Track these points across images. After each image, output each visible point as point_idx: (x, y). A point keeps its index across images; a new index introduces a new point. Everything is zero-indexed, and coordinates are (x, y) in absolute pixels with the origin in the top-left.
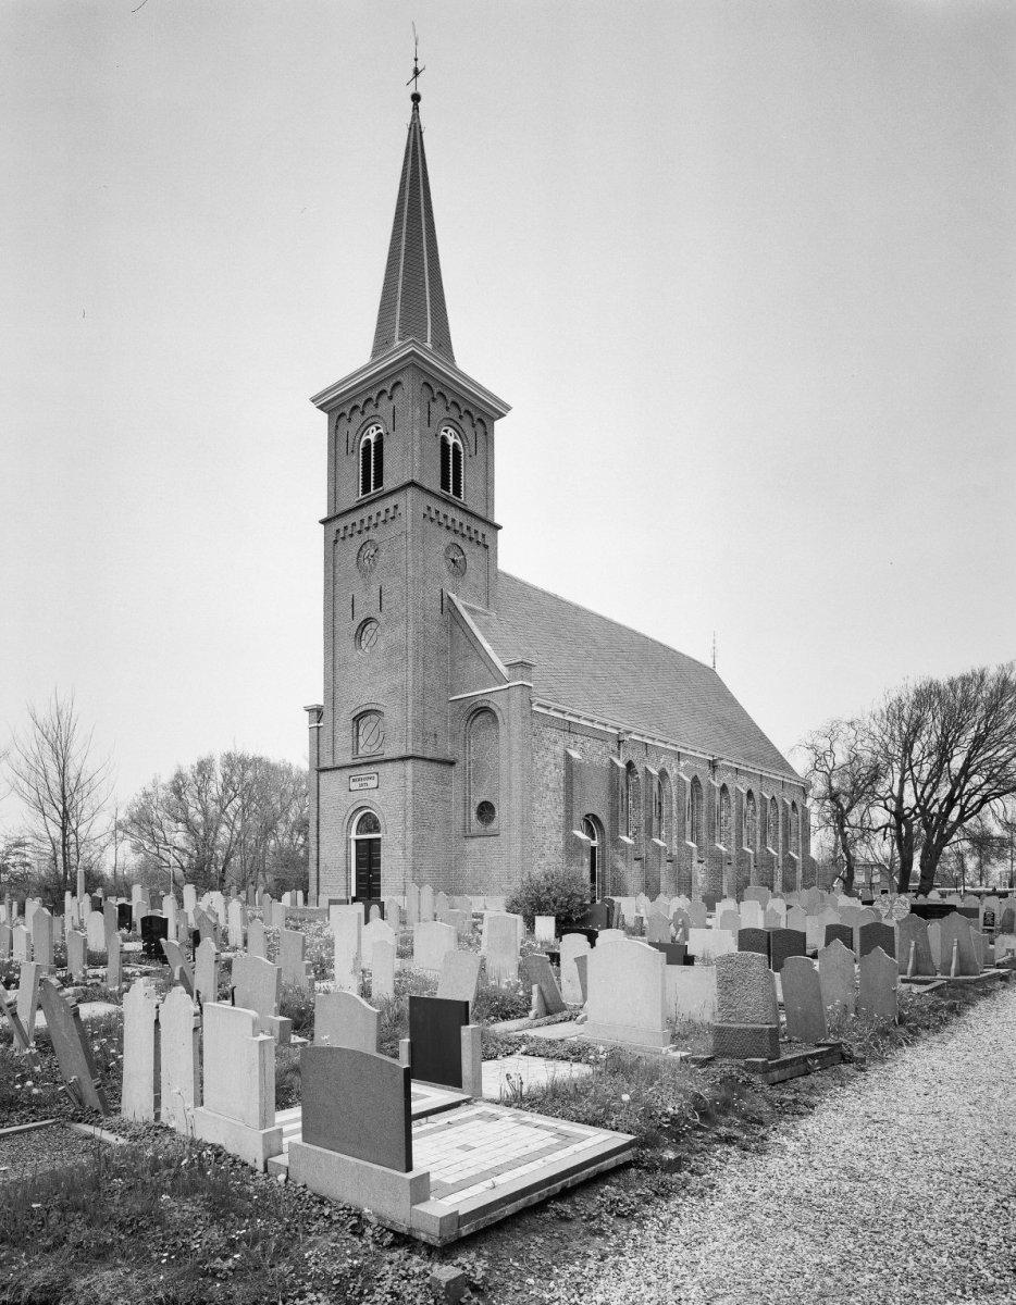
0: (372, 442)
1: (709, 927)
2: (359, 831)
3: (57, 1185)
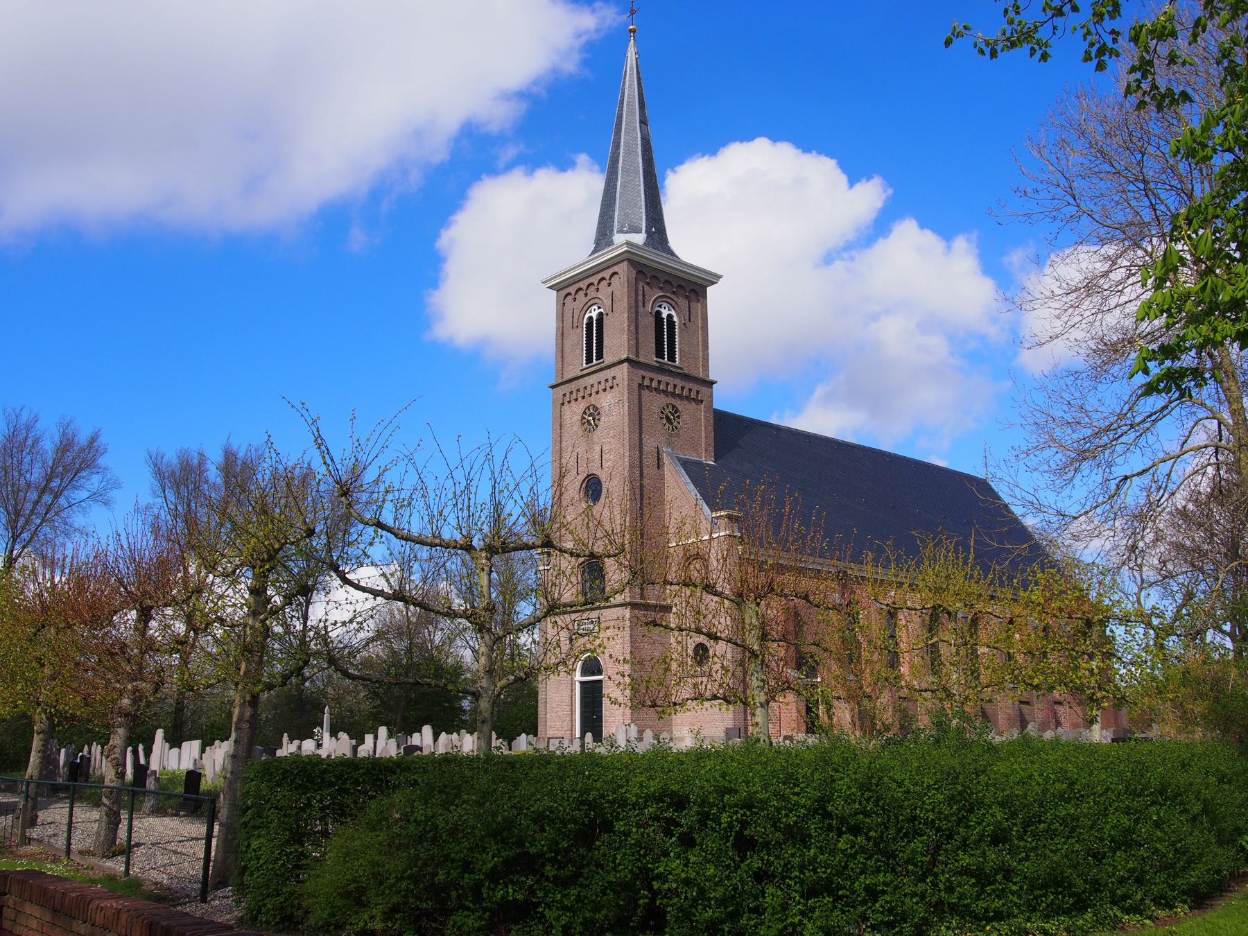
2: (584, 673)
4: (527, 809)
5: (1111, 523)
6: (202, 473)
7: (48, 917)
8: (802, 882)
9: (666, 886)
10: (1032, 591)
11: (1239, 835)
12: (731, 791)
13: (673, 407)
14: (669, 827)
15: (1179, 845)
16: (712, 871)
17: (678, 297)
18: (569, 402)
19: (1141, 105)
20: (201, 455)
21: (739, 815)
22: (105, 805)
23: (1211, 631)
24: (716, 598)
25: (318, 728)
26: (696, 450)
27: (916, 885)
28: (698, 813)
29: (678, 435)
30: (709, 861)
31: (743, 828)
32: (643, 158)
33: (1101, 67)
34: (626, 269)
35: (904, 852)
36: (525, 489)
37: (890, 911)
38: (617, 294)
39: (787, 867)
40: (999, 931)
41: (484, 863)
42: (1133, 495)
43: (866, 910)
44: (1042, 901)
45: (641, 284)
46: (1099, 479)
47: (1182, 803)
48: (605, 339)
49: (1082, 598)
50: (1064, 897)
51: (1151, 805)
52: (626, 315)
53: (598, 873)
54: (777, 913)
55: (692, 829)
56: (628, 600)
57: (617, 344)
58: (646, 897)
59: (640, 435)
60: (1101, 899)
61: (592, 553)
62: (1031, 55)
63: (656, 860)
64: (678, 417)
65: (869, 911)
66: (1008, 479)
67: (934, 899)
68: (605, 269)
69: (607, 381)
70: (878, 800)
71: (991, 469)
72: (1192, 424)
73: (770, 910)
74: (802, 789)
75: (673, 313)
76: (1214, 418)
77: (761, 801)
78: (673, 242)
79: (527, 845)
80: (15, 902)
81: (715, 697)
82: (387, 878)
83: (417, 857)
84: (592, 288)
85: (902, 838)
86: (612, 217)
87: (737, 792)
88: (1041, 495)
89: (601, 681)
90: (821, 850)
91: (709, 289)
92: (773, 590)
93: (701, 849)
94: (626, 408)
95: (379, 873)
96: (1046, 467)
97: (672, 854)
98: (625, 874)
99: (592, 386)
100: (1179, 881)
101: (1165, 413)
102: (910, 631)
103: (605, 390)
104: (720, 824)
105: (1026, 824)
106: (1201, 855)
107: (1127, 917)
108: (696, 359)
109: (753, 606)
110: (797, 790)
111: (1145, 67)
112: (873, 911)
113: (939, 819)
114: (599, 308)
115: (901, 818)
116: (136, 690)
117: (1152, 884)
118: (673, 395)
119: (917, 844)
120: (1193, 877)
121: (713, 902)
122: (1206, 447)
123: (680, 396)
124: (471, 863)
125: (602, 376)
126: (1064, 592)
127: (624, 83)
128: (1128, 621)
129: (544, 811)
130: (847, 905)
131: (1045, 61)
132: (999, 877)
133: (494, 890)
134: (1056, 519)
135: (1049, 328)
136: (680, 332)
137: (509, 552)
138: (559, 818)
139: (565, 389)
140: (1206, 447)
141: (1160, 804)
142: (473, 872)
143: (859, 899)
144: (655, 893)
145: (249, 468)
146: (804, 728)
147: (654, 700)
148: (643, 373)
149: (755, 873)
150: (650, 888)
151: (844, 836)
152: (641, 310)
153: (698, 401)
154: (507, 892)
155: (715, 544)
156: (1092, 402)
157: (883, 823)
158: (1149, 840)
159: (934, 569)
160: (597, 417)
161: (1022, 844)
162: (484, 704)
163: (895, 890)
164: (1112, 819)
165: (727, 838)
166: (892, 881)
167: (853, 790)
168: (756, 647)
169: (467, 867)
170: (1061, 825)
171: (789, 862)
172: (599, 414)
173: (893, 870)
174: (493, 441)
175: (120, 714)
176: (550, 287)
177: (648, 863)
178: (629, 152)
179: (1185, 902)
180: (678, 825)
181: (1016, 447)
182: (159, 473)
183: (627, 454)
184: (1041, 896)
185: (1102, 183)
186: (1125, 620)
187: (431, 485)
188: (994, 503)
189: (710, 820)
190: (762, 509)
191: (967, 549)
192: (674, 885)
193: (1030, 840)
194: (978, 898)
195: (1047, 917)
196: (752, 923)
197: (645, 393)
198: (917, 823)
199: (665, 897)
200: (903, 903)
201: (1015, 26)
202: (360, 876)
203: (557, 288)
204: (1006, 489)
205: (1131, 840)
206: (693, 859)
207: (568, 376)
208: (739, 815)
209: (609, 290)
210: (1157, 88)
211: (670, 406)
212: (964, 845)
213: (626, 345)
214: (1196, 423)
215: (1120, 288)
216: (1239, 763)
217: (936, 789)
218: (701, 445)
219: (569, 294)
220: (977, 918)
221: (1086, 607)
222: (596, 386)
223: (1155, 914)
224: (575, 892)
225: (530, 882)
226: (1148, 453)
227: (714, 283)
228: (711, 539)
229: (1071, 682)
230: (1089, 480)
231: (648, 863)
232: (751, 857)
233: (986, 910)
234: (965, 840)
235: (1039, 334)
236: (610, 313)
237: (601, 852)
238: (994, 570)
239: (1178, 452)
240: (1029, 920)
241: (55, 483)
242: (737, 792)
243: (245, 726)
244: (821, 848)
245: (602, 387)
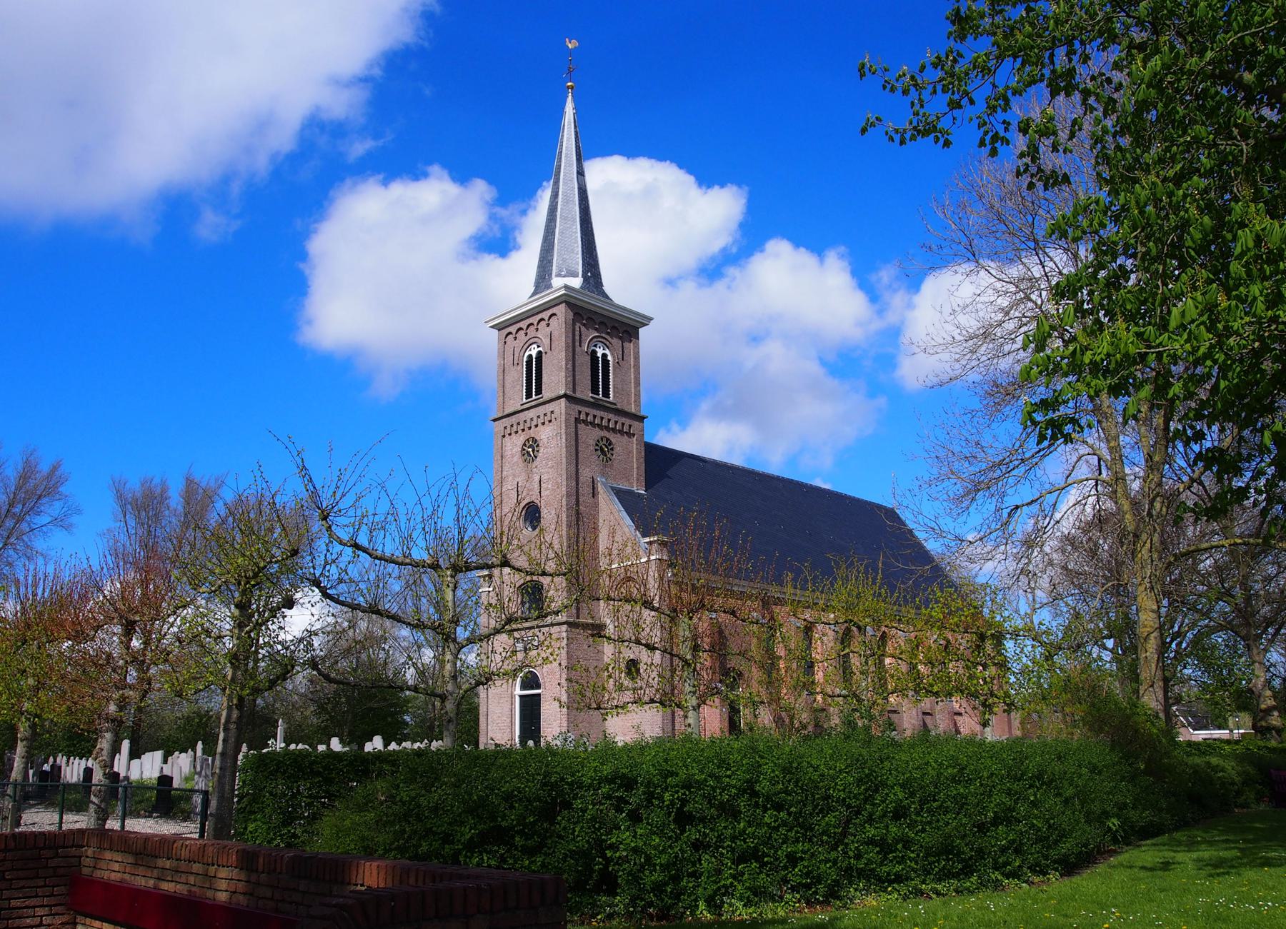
0: (534, 356)
1: (948, 38)
2: (524, 687)
3: (174, 815)
4: (499, 789)
5: (1003, 547)
6: (161, 502)
7: (131, 859)
8: (733, 850)
9: (618, 855)
10: (933, 608)
11: (1107, 818)
12: (673, 774)
13: (607, 439)
14: (620, 804)
15: (1052, 821)
16: (657, 840)
17: (612, 338)
18: (510, 434)
19: (1031, 186)
20: (163, 483)
21: (680, 794)
22: (94, 803)
24: (653, 613)
25: (272, 740)
26: (628, 480)
27: (829, 853)
28: (644, 793)
29: (611, 466)
30: (654, 833)
31: (683, 805)
32: (580, 207)
33: (994, 153)
34: (564, 311)
35: (819, 825)
36: (484, 514)
37: (808, 875)
38: (556, 334)
39: (720, 839)
40: (899, 891)
41: (463, 835)
42: (1024, 524)
43: (787, 874)
44: (935, 867)
45: (578, 325)
46: (992, 508)
47: (1057, 788)
48: (544, 375)
49: (977, 614)
50: (953, 864)
51: (1029, 788)
52: (563, 354)
53: (560, 843)
54: (713, 876)
55: (639, 806)
56: (565, 619)
57: (555, 382)
58: (601, 864)
59: (577, 466)
60: (985, 865)
61: (544, 572)
62: (936, 142)
63: (609, 833)
64: (612, 449)
65: (790, 875)
66: (913, 507)
67: (844, 865)
68: (544, 310)
69: (545, 415)
70: (797, 781)
71: (898, 498)
72: (1074, 459)
73: (706, 874)
74: (733, 772)
75: (607, 352)
76: (1094, 454)
77: (697, 782)
78: (608, 287)
79: (499, 819)
80: (94, 852)
81: (652, 701)
82: (377, 850)
83: (403, 831)
84: (532, 328)
85: (817, 813)
86: (550, 262)
87: (677, 775)
88: (941, 522)
90: (749, 824)
92: (704, 605)
93: (648, 823)
94: (564, 440)
95: (368, 847)
96: (945, 497)
97: (622, 828)
98: (582, 842)
99: (532, 419)
100: (1052, 852)
101: (1052, 449)
102: (825, 643)
103: (543, 424)
104: (663, 802)
105: (922, 802)
106: (1071, 831)
107: (1007, 881)
108: (629, 395)
109: (686, 620)
110: (728, 773)
111: (1033, 152)
112: (793, 875)
113: (849, 798)
114: (538, 346)
115: (817, 796)
116: (124, 698)
117: (1028, 854)
118: (607, 428)
119: (830, 818)
120: (1065, 847)
121: (658, 868)
122: (1087, 480)
123: (614, 430)
124: (451, 835)
125: (541, 410)
126: (962, 610)
127: (563, 136)
128: (1017, 635)
129: (513, 791)
130: (771, 869)
131: (948, 147)
132: (900, 846)
133: (470, 858)
134: (953, 544)
135: (949, 370)
136: (614, 370)
137: (471, 570)
138: (525, 797)
139: (506, 422)
140: (1087, 480)
141: (1037, 787)
142: (453, 843)
143: (782, 865)
144: (608, 861)
145: (210, 497)
147: (599, 703)
148: (579, 408)
149: (693, 844)
150: (604, 856)
151: (769, 812)
152: (578, 349)
153: (630, 435)
154: (482, 859)
155: (653, 563)
156: (987, 439)
157: (802, 801)
158: (1027, 817)
159: (846, 588)
160: (536, 449)
161: (919, 819)
162: (449, 706)
163: (811, 857)
164: (997, 799)
165: (669, 814)
166: (809, 850)
167: (777, 773)
168: (689, 657)
169: (447, 839)
170: (952, 803)
171: (722, 834)
172: (538, 446)
173: (810, 840)
174: (457, 472)
175: (107, 720)
176: (492, 327)
177: (602, 835)
178: (567, 202)
179: (1056, 870)
180: (627, 803)
181: (920, 477)
182: (120, 496)
183: (564, 483)
184: (934, 862)
185: (998, 243)
186: (1015, 635)
187: (402, 511)
188: (900, 529)
189: (655, 798)
190: (694, 533)
191: (875, 570)
192: (625, 854)
193: (925, 815)
194: (881, 864)
195: (939, 880)
196: (691, 885)
197: (581, 426)
198: (830, 801)
199: (617, 863)
200: (818, 868)
201: (920, 117)
202: (351, 850)
203: (499, 327)
204: (910, 516)
205: (1012, 816)
206: (639, 831)
207: (508, 411)
208: (680, 794)
209: (548, 330)
210: (1042, 171)
211: (604, 439)
212: (870, 820)
213: (564, 381)
214: (1079, 459)
215: (1013, 336)
216: (1108, 758)
217: (846, 773)
218: (633, 475)
219: (510, 333)
220: (880, 880)
221: (978, 623)
222: (535, 419)
223: (1030, 879)
224: (541, 859)
225: (501, 851)
226: (1037, 485)
228: (649, 561)
229: (966, 689)
230: (983, 510)
231: (602, 835)
232: (689, 831)
233: (889, 874)
234: (871, 815)
235: (941, 374)
236: (549, 351)
237: (562, 825)
238: (900, 589)
239: (1063, 485)
240: (924, 882)
241: (17, 509)
242: (677, 775)
243: (232, 726)
244: (749, 822)
245: (541, 420)
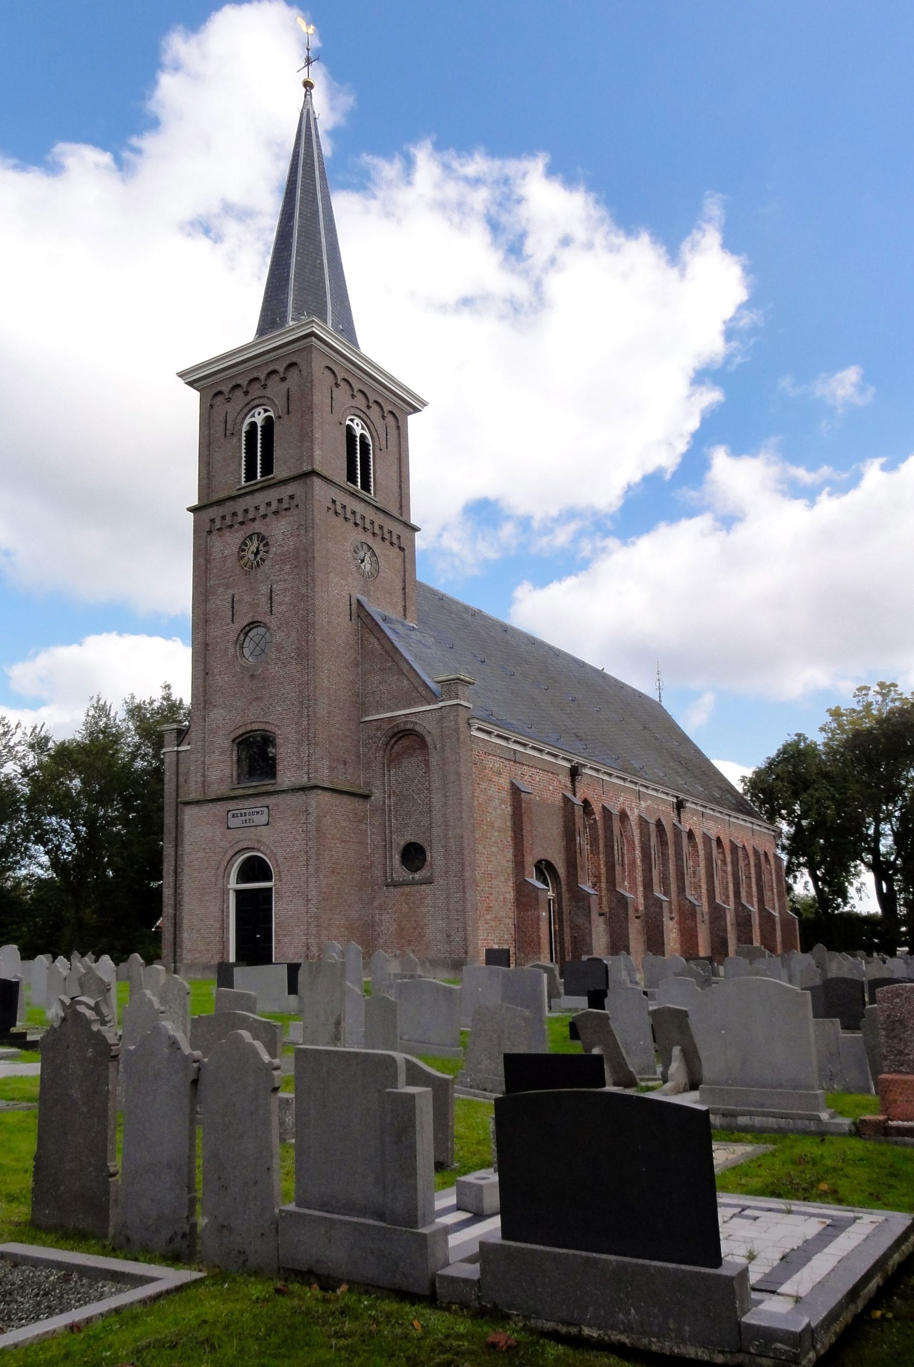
23: (302, 1023)
89: (270, 889)
91: (411, 418)
103: (276, 513)
114: (266, 411)
125: (272, 495)
139: (214, 512)
146: (656, 995)
209: (284, 386)
227: (416, 410)
